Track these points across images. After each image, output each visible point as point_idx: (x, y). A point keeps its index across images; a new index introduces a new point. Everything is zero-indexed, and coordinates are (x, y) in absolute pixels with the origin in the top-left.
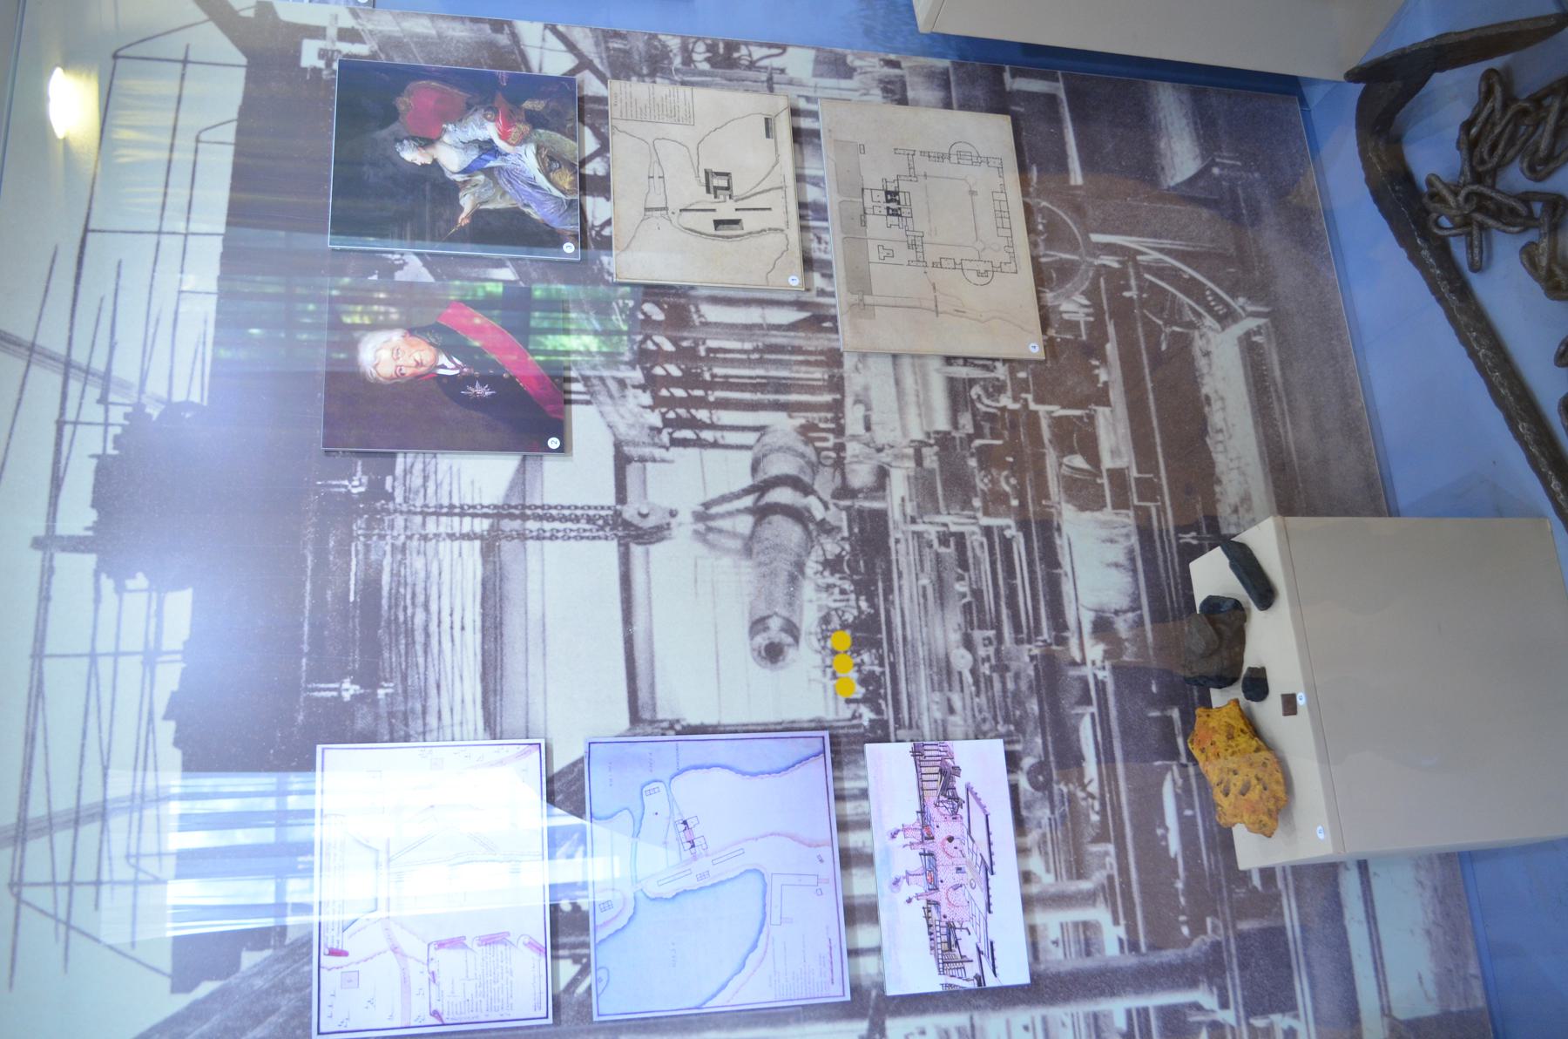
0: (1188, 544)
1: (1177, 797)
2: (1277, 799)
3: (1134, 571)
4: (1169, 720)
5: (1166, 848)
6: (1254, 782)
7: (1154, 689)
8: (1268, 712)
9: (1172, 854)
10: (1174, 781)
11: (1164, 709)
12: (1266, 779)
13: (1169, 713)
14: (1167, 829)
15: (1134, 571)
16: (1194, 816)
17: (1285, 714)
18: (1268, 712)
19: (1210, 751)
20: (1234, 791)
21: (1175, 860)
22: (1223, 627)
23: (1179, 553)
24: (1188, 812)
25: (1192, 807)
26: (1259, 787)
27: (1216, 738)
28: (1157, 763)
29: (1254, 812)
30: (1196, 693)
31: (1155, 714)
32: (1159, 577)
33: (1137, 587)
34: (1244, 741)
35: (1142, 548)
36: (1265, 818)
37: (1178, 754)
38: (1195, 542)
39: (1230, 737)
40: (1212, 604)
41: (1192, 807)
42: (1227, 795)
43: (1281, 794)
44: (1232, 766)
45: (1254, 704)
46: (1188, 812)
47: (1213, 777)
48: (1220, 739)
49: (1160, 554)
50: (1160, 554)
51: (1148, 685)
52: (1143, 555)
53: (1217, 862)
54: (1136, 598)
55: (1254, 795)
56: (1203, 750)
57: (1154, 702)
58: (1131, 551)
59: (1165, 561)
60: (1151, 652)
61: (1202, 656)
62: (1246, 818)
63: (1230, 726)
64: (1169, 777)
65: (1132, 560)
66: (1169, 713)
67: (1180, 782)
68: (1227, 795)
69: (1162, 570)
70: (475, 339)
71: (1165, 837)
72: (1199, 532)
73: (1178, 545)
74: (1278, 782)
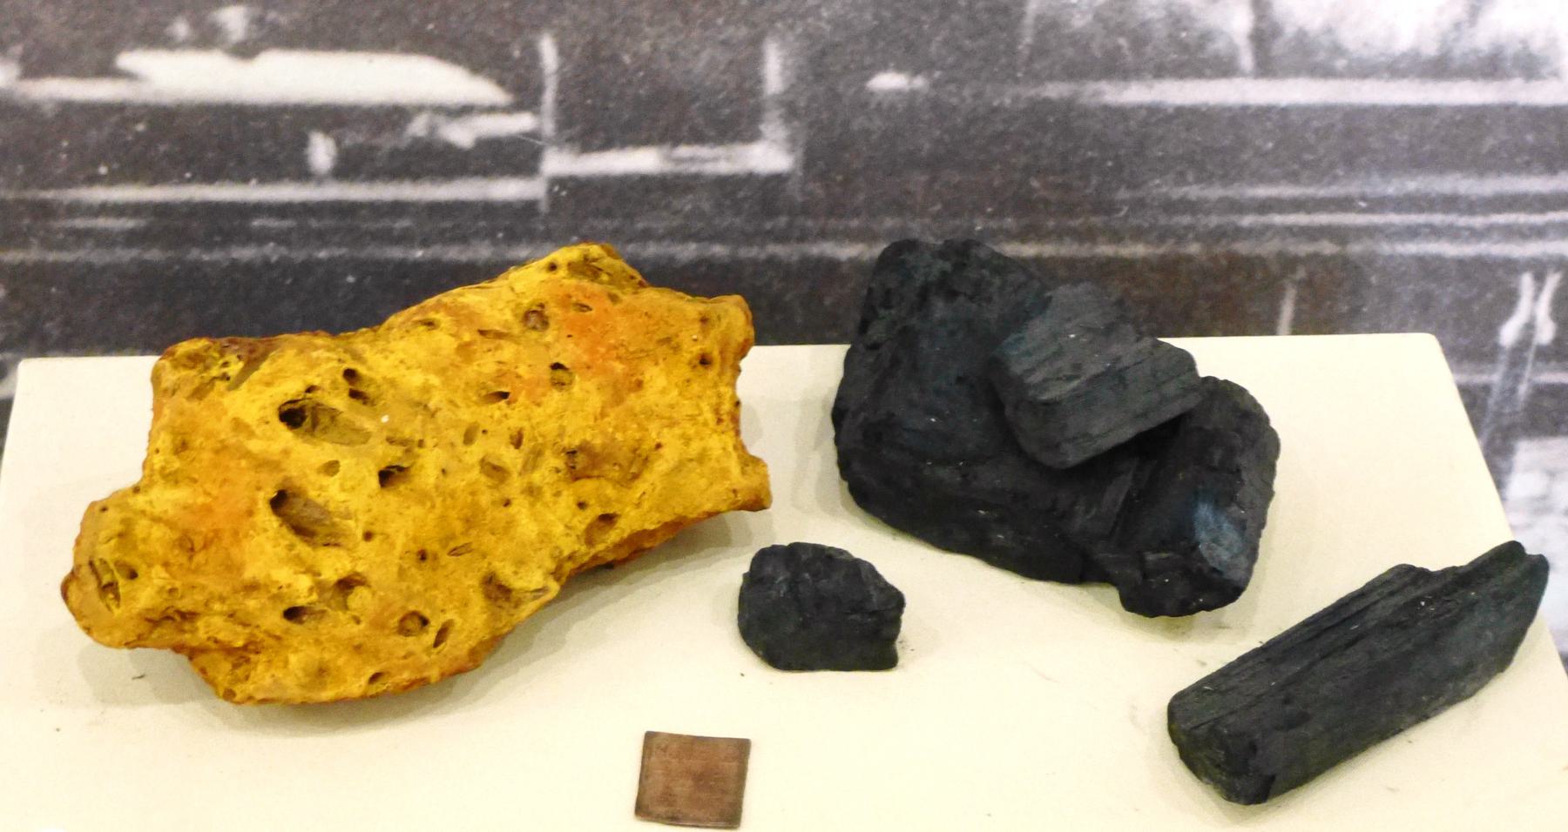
0: (1509, 300)
1: (394, 116)
2: (242, 655)
3: (1439, 68)
4: (737, 125)
5: (155, 38)
6: (333, 565)
7: (888, 82)
8: (678, 655)
9: (129, 60)
10: (463, 111)
11: (791, 111)
12: (339, 625)
13: (774, 128)
14: (245, 51)
15: (1439, 68)
16: (303, 174)
17: (650, 737)
18: (678, 655)
19: (524, 358)
20: (304, 456)
21: (106, 70)
22: (1116, 494)
23: (1481, 262)
24: (322, 152)
25: (347, 168)
26: (301, 589)
27: (587, 391)
28: (548, 51)
29: (187, 544)
30: (847, 252)
31: (775, 70)
32: (1387, 168)
33: (1364, 70)
34: (549, 524)
35: (1538, 116)
36: (145, 595)
37: (591, 137)
38: (1509, 333)
39: (581, 463)
40: (1224, 448)
41: (347, 168)
42: (292, 416)
43: (262, 677)
44: (428, 466)
45: (731, 571)
46: (322, 152)
47: (401, 353)
48: (576, 414)
49: (1491, 186)
50: (1491, 186)
51: (911, 61)
52: (1506, 112)
53: (105, 239)
54: (1312, 57)
55: (268, 554)
56: (535, 317)
57: (823, 66)
58: (1530, 66)
59: (1451, 203)
60: (1055, 90)
61: (996, 365)
62: (165, 499)
63: (638, 461)
64: (483, 90)
65: (1491, 66)
66: (774, 128)
67: (461, 135)
68: (292, 416)
69: (1412, 185)
70: (319, 248)
71: (207, 38)
72: (1549, 355)
73: (1513, 267)
74: (321, 673)
